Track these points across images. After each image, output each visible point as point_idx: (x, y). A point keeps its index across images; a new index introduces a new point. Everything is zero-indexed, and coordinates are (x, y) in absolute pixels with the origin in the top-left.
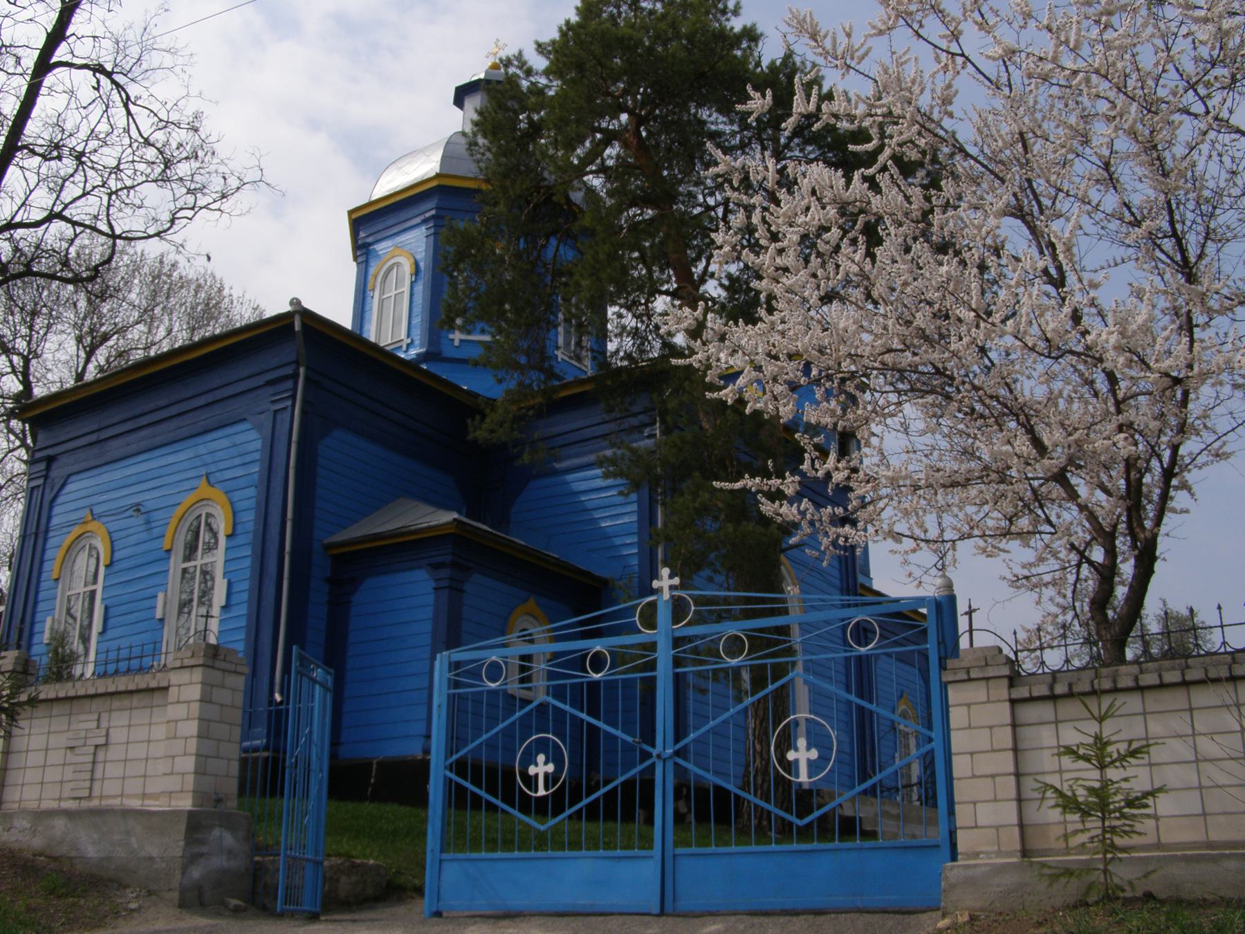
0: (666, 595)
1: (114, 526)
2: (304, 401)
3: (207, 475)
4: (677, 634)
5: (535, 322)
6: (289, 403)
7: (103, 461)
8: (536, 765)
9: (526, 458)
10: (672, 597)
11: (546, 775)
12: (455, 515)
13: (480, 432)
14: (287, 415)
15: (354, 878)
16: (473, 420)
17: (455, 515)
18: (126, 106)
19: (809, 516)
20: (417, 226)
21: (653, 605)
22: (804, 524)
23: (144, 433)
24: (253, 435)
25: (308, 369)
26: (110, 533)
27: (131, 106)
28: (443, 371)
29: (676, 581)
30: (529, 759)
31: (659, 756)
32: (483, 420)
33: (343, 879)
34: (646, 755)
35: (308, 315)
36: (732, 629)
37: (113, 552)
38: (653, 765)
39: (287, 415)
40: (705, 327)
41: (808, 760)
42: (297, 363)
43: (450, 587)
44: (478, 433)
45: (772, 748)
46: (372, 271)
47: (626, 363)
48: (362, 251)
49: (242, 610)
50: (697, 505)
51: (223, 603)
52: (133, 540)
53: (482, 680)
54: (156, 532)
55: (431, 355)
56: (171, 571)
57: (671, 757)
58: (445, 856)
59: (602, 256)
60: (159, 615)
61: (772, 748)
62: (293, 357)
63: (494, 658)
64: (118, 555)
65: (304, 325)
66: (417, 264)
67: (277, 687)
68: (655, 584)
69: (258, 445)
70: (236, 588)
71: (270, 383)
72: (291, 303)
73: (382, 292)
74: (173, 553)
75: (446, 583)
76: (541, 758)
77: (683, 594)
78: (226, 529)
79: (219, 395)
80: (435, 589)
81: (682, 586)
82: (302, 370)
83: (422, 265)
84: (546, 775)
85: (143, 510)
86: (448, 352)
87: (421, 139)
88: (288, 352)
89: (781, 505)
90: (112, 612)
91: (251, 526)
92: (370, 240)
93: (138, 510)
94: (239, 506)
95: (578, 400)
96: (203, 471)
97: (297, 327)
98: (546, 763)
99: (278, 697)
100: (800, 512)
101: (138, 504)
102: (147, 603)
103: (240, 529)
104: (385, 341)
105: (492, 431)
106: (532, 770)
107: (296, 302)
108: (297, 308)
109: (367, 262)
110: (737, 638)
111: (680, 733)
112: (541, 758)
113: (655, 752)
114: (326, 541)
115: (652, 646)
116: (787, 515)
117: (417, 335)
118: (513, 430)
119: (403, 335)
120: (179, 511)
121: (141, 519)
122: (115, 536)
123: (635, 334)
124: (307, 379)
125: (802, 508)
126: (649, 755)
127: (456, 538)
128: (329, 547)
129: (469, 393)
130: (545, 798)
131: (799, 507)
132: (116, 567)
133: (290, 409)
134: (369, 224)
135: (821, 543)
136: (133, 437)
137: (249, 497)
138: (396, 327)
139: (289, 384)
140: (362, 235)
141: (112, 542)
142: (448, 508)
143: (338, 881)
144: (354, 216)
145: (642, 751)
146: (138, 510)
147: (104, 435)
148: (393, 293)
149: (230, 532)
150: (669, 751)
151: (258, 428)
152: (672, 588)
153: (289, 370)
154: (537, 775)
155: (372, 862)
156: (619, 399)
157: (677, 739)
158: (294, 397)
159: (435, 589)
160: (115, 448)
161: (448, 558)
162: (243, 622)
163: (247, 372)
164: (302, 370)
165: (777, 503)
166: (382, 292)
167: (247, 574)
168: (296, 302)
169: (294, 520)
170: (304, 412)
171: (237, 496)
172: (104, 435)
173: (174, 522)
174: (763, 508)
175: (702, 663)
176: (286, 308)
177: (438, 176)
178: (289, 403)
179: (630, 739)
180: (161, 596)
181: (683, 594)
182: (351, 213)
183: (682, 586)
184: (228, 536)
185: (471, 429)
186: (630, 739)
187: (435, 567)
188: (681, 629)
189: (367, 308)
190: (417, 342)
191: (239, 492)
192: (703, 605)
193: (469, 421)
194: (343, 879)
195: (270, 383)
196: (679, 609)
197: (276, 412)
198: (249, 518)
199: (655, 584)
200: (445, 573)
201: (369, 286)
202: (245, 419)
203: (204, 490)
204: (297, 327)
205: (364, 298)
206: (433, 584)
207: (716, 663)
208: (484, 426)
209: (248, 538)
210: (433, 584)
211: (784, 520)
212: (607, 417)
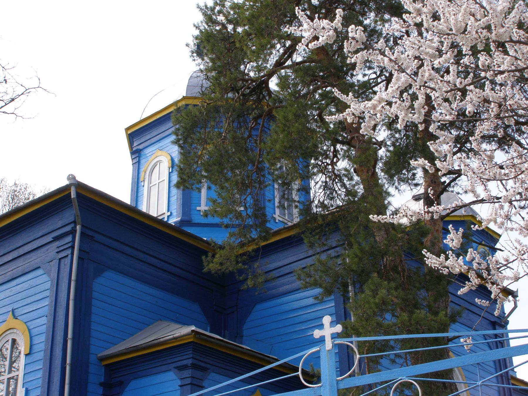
0: (329, 345)
2: (80, 250)
3: (13, 311)
4: (342, 386)
5: (253, 183)
6: (69, 252)
10: (334, 345)
12: (193, 328)
13: (212, 265)
14: (67, 261)
17: (193, 328)
19: (475, 265)
20: (170, 135)
22: (472, 275)
24: (45, 278)
25: (83, 226)
29: (339, 328)
32: (213, 256)
35: (81, 187)
39: (67, 261)
43: (191, 384)
44: (211, 265)
46: (142, 169)
47: (319, 210)
48: (136, 154)
50: (377, 301)
59: (291, 116)
62: (72, 219)
65: (78, 194)
66: (172, 160)
68: (317, 334)
69: (48, 285)
71: (56, 239)
72: (68, 179)
75: (188, 381)
78: (25, 350)
79: (21, 251)
80: (180, 386)
81: (345, 334)
82: (78, 228)
83: (176, 161)
87: (173, 74)
88: (70, 215)
91: (42, 346)
92: (141, 147)
95: (289, 241)
97: (73, 195)
100: (465, 263)
103: (36, 348)
104: (154, 213)
105: (221, 264)
107: (72, 177)
108: (73, 182)
110: (408, 385)
114: (99, 355)
118: (237, 262)
124: (82, 234)
125: (468, 258)
127: (196, 346)
128: (102, 359)
133: (70, 256)
134: (140, 136)
135: (490, 293)
137: (42, 324)
138: (159, 201)
139: (69, 238)
140: (135, 144)
142: (189, 324)
144: (129, 132)
151: (48, 273)
152: (335, 336)
153: (68, 228)
156: (317, 237)
158: (73, 247)
159: (180, 386)
161: (189, 362)
163: (41, 234)
164: (78, 228)
165: (443, 256)
168: (72, 177)
169: (73, 339)
170: (80, 258)
171: (32, 325)
176: (64, 182)
177: (184, 98)
178: (69, 252)
182: (127, 129)
183: (345, 334)
184: (26, 355)
185: (205, 264)
187: (181, 368)
189: (140, 194)
190: (175, 214)
195: (56, 239)
196: (344, 358)
199: (317, 334)
200: (187, 373)
201: (141, 179)
202: (39, 267)
203: (11, 322)
204: (73, 195)
205: (138, 188)
206: (179, 382)
208: (215, 260)
210: (179, 382)
211: (450, 273)
212: (311, 252)
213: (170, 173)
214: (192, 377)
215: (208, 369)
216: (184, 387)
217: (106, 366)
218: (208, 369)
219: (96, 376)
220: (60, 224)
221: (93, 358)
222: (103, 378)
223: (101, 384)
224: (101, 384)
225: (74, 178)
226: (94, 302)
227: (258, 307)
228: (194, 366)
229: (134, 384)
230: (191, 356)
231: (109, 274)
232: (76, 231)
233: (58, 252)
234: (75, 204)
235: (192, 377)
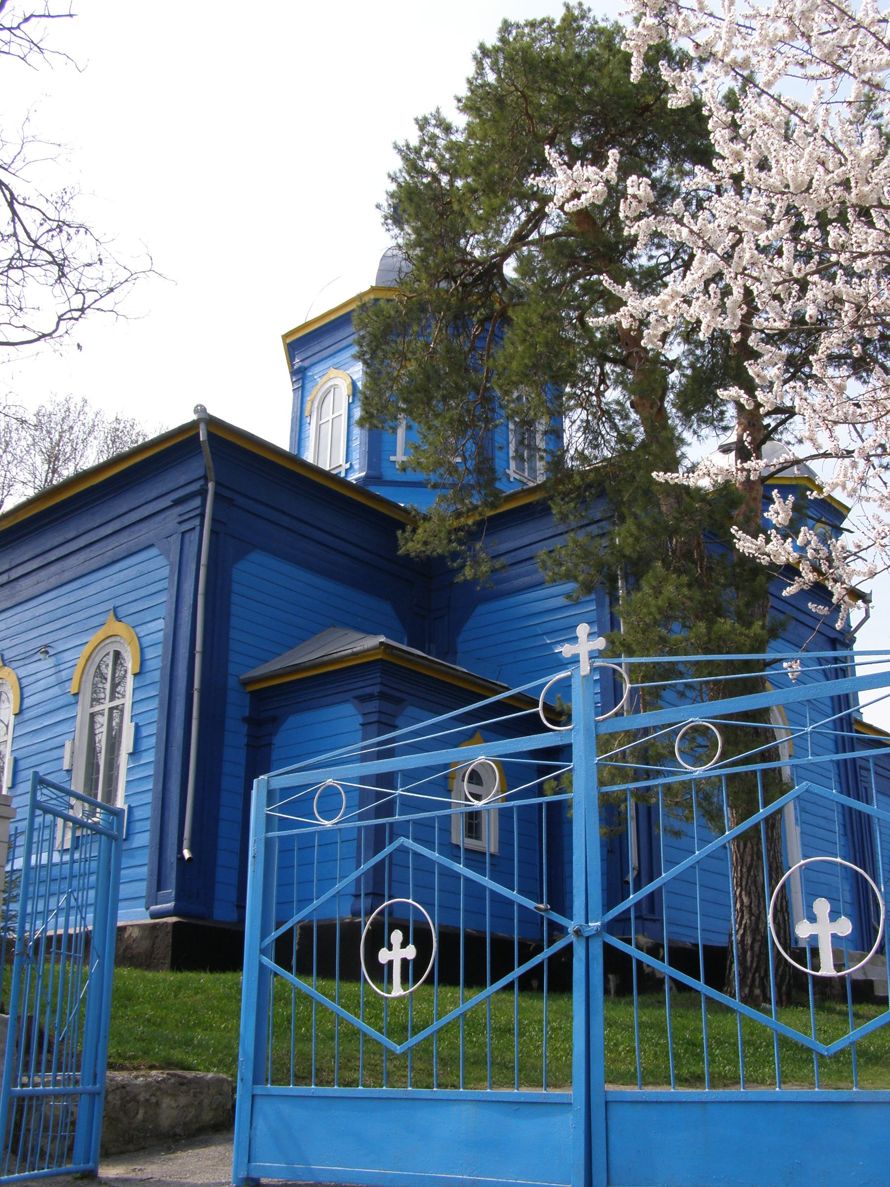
0: (585, 668)
1: (22, 672)
2: (214, 520)
3: (115, 608)
4: (604, 730)
6: (197, 522)
7: (14, 602)
8: (390, 948)
9: (468, 573)
10: (593, 669)
11: (405, 962)
13: (411, 545)
14: (195, 535)
15: (183, 1100)
16: (404, 531)
17: (383, 639)
18: (11, 205)
19: (810, 553)
21: (565, 685)
23: (53, 569)
24: (162, 561)
25: (218, 484)
26: (19, 679)
27: (16, 206)
28: (378, 491)
30: (378, 940)
31: (578, 933)
32: (414, 531)
33: (166, 1102)
34: (556, 930)
35: (213, 423)
36: (694, 715)
37: (22, 699)
38: (569, 948)
39: (195, 535)
40: (624, 195)
41: (834, 936)
42: (205, 478)
43: (378, 722)
44: (410, 544)
45: (770, 917)
48: (300, 375)
49: (149, 757)
50: (660, 603)
51: (131, 751)
52: (42, 684)
53: (311, 815)
54: (64, 675)
55: (374, 477)
56: (79, 717)
57: (598, 934)
58: (259, 1089)
60: (66, 766)
61: (770, 917)
62: (201, 472)
63: (330, 781)
64: (27, 702)
65: (210, 435)
66: (354, 384)
67: (186, 843)
70: (145, 732)
71: (177, 503)
72: (196, 411)
73: (320, 417)
74: (81, 697)
75: (375, 718)
76: (397, 936)
77: (610, 663)
82: (211, 486)
84: (405, 962)
85: (52, 652)
86: (390, 475)
87: (353, 252)
89: (768, 541)
90: (22, 764)
92: (306, 364)
93: (47, 652)
94: (146, 641)
95: (531, 510)
96: (110, 605)
98: (404, 945)
99: (187, 854)
100: (796, 548)
101: (46, 646)
102: (55, 754)
106: (384, 956)
107: (200, 410)
109: (303, 387)
111: (615, 889)
112: (397, 936)
113: (572, 926)
114: (242, 677)
115: (562, 752)
116: (777, 554)
117: (356, 456)
118: (450, 541)
119: (341, 460)
120: (87, 650)
121: (49, 662)
122: (25, 682)
123: (586, 428)
124: (217, 495)
125: (800, 541)
126: (563, 930)
127: (384, 666)
129: (404, 510)
130: (400, 999)
131: (794, 541)
132: (27, 715)
133: (198, 528)
134: (306, 347)
135: (831, 594)
136: (43, 574)
138: (333, 447)
139: (197, 502)
141: (21, 689)
142: (376, 633)
143: (157, 1104)
144: (288, 341)
145: (552, 925)
146: (47, 652)
147: (15, 574)
148: (330, 418)
149: (137, 670)
150: (595, 924)
151: (165, 553)
154: (391, 963)
155: (210, 1075)
157: (609, 903)
158: (202, 515)
160: (26, 587)
161: (376, 689)
162: (150, 771)
163: (154, 494)
164: (211, 486)
165: (762, 537)
166: (320, 417)
167: (155, 716)
168: (200, 410)
170: (213, 532)
171: (143, 630)
172: (15, 574)
173: (81, 663)
174: (739, 545)
175: (648, 775)
176: (193, 417)
177: (373, 289)
178: (197, 522)
179: (531, 904)
180: (68, 745)
181: (610, 663)
182: (285, 337)
184: (135, 675)
185: (401, 542)
186: (531, 904)
187: (363, 699)
188: (609, 721)
190: (356, 467)
191: (144, 627)
192: (645, 679)
193: (399, 532)
194: (166, 1102)
195: (177, 503)
196: (609, 688)
197: (183, 533)
198: (156, 657)
200: (373, 706)
201: (307, 413)
205: (301, 426)
206: (361, 720)
207: (673, 773)
208: (416, 537)
209: (156, 676)
210: (361, 720)
213: (349, 404)
214: (379, 712)
215: (404, 700)
216: (369, 727)
217: (251, 692)
218: (404, 700)
219: (237, 707)
220: (183, 480)
221: (232, 682)
222: (248, 710)
223: (245, 720)
224: (245, 720)
225: (204, 410)
226: (235, 598)
227: (480, 609)
228: (382, 696)
229: (293, 721)
230: (379, 680)
231: (256, 556)
232: (207, 491)
233: (180, 523)
234: (206, 449)
235: (379, 712)
